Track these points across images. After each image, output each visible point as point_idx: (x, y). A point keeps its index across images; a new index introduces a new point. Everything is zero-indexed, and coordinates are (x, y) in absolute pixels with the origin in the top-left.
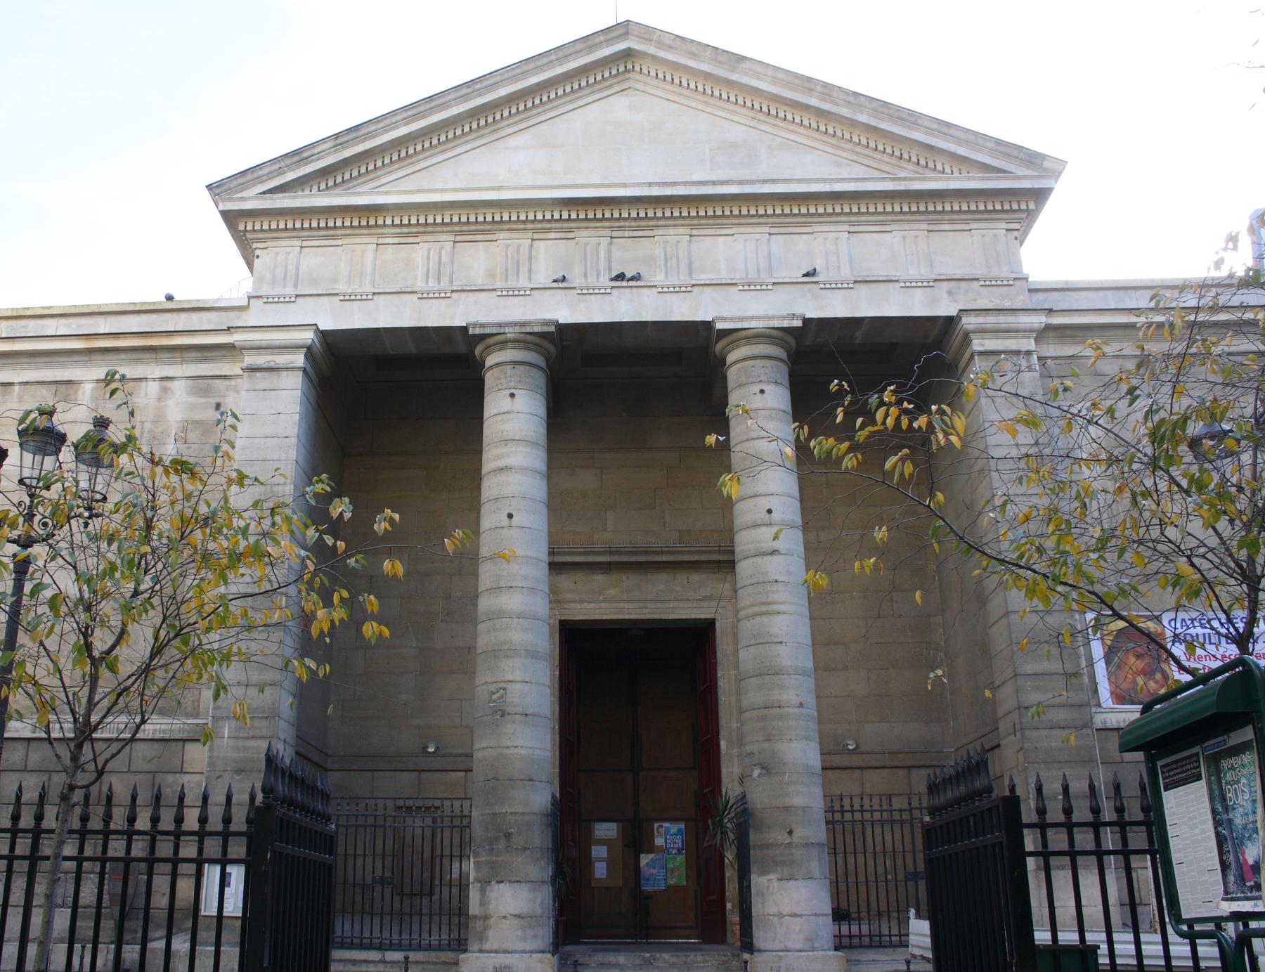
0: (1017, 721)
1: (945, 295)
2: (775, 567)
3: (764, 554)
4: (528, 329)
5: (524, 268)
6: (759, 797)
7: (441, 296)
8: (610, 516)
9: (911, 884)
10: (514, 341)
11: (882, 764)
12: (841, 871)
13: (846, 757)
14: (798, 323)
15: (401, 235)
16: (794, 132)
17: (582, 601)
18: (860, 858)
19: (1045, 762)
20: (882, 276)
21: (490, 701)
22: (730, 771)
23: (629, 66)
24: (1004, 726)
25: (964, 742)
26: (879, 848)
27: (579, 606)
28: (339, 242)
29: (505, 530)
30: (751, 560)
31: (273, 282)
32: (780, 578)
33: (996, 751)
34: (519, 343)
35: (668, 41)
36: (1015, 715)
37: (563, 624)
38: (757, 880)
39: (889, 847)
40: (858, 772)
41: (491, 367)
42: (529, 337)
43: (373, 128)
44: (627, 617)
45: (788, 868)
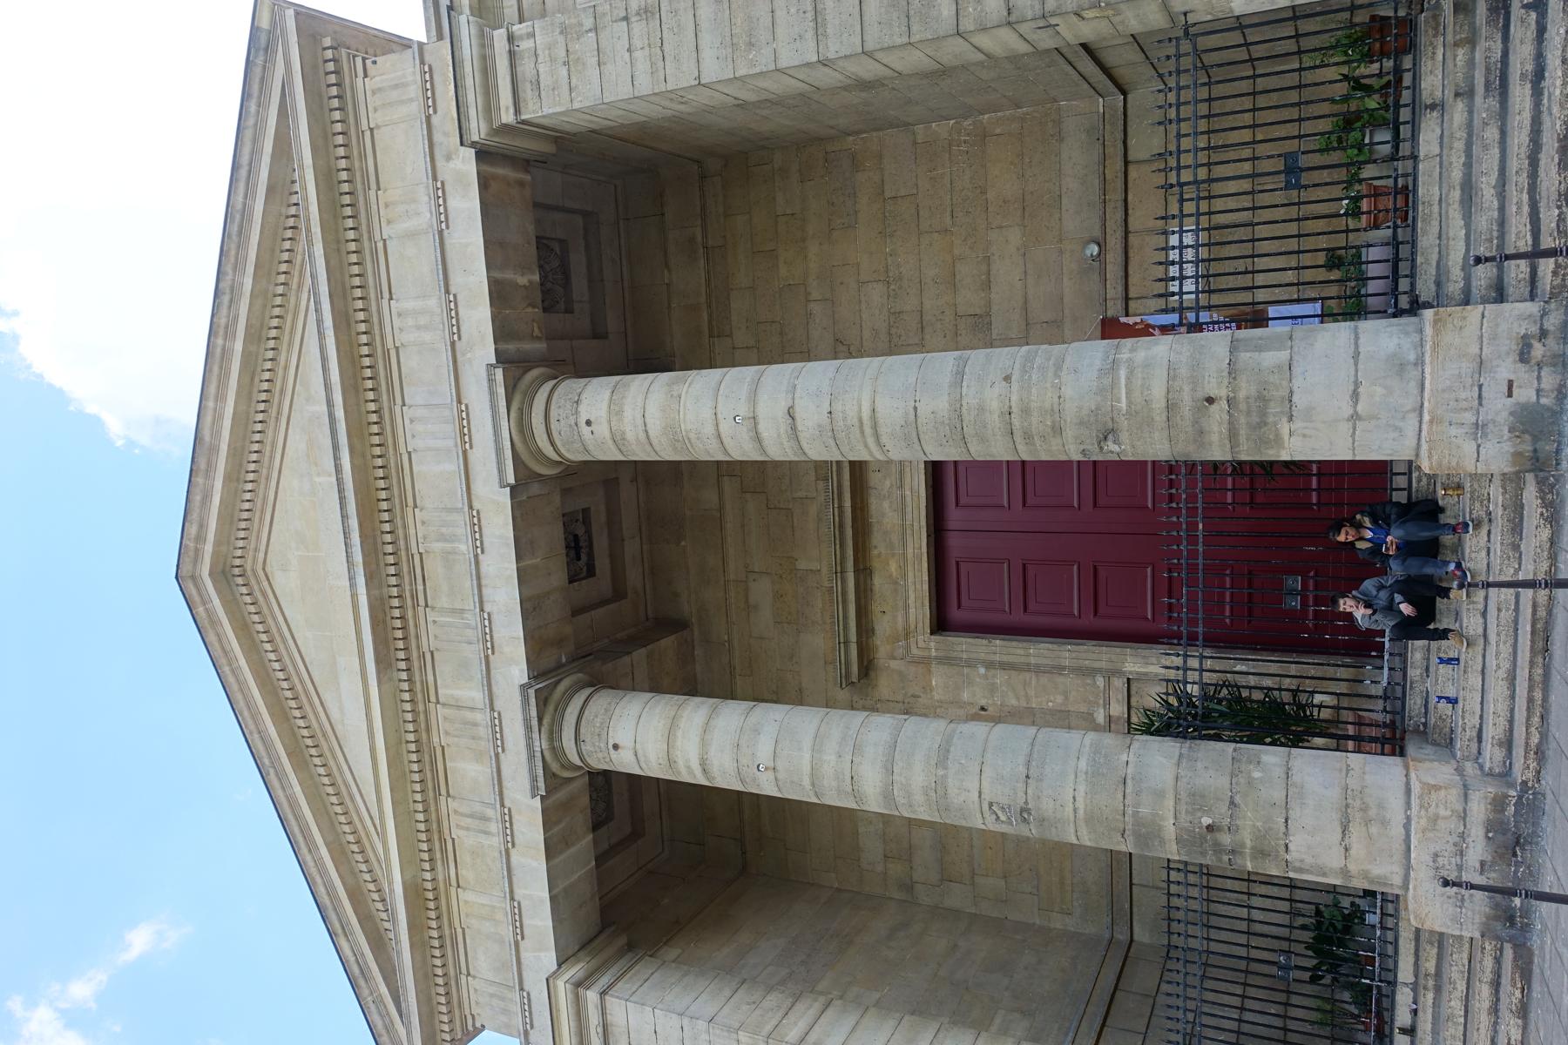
0: (1033, 24)
1: (451, 165)
2: (811, 416)
3: (794, 428)
4: (535, 722)
5: (469, 715)
8: (802, 565)
9: (1306, 178)
10: (551, 739)
11: (1120, 204)
15: (445, 860)
16: (286, 368)
17: (906, 607)
18: (1262, 231)
20: (440, 261)
23: (237, 571)
24: (1046, 41)
26: (1246, 202)
27: (912, 611)
28: (459, 931)
29: (780, 776)
31: (505, 1011)
32: (826, 407)
34: (554, 735)
35: (193, 530)
36: (1024, 28)
39: (1245, 185)
40: (1131, 238)
42: (546, 721)
43: (321, 890)
44: (924, 550)
45: (1267, 405)
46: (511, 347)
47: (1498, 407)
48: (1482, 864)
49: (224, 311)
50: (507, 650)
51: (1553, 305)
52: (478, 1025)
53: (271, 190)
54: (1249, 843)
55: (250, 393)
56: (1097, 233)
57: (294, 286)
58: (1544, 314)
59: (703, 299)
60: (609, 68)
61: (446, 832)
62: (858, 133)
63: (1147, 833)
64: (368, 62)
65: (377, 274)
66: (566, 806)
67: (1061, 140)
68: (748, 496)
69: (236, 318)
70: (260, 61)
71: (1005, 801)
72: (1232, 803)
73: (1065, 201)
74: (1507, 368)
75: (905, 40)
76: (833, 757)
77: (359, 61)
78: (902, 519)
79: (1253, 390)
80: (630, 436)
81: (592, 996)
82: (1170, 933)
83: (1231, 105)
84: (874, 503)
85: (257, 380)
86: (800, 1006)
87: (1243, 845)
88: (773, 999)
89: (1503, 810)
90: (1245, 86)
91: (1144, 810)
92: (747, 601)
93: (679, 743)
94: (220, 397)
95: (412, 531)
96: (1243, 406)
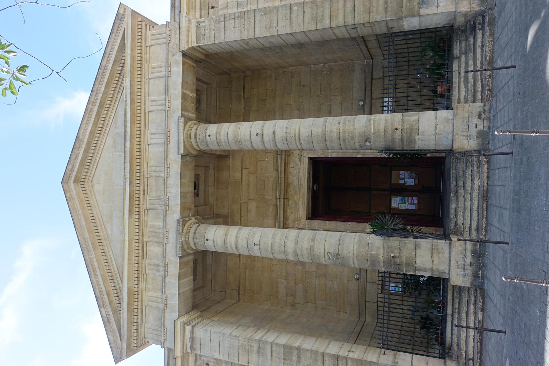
1: (174, 57)
3: (274, 137)
6: (381, 143)
7: (166, 267)
8: (266, 197)
12: (457, 301)
13: (366, 105)
14: (182, 120)
16: (110, 118)
19: (370, 13)
20: (167, 85)
21: (333, 259)
22: (370, 154)
24: (354, 35)
25: (362, 55)
30: (277, 143)
32: (285, 131)
33: (366, 39)
35: (70, 167)
36: (348, 28)
37: (309, 218)
38: (416, 149)
41: (196, 247)
46: (186, 114)
47: (473, 132)
48: (471, 263)
49: (93, 97)
50: (173, 208)
51: (487, 104)
52: (146, 341)
53: (115, 61)
54: (404, 261)
55: (97, 124)
56: (363, 98)
57: (117, 92)
58: (484, 106)
59: (242, 113)
60: (227, 32)
61: (144, 271)
62: (294, 66)
63: (374, 261)
64: (151, 27)
65: (145, 89)
66: (186, 263)
67: (354, 72)
68: (251, 175)
69: (97, 99)
70: (118, 23)
71: (332, 252)
72: (400, 249)
73: (354, 89)
74: (475, 120)
75: (315, 28)
76: (279, 240)
77: (148, 26)
78: (300, 174)
79: (408, 126)
80: (222, 140)
81: (189, 328)
82: (378, 318)
83: (402, 64)
84: (291, 177)
85: (100, 120)
86: (259, 331)
87: (403, 262)
88: (250, 329)
89: (476, 247)
90: (406, 59)
91: (374, 252)
92: (247, 209)
93: (228, 238)
94: (87, 124)
95: (146, 170)
96: (405, 131)
